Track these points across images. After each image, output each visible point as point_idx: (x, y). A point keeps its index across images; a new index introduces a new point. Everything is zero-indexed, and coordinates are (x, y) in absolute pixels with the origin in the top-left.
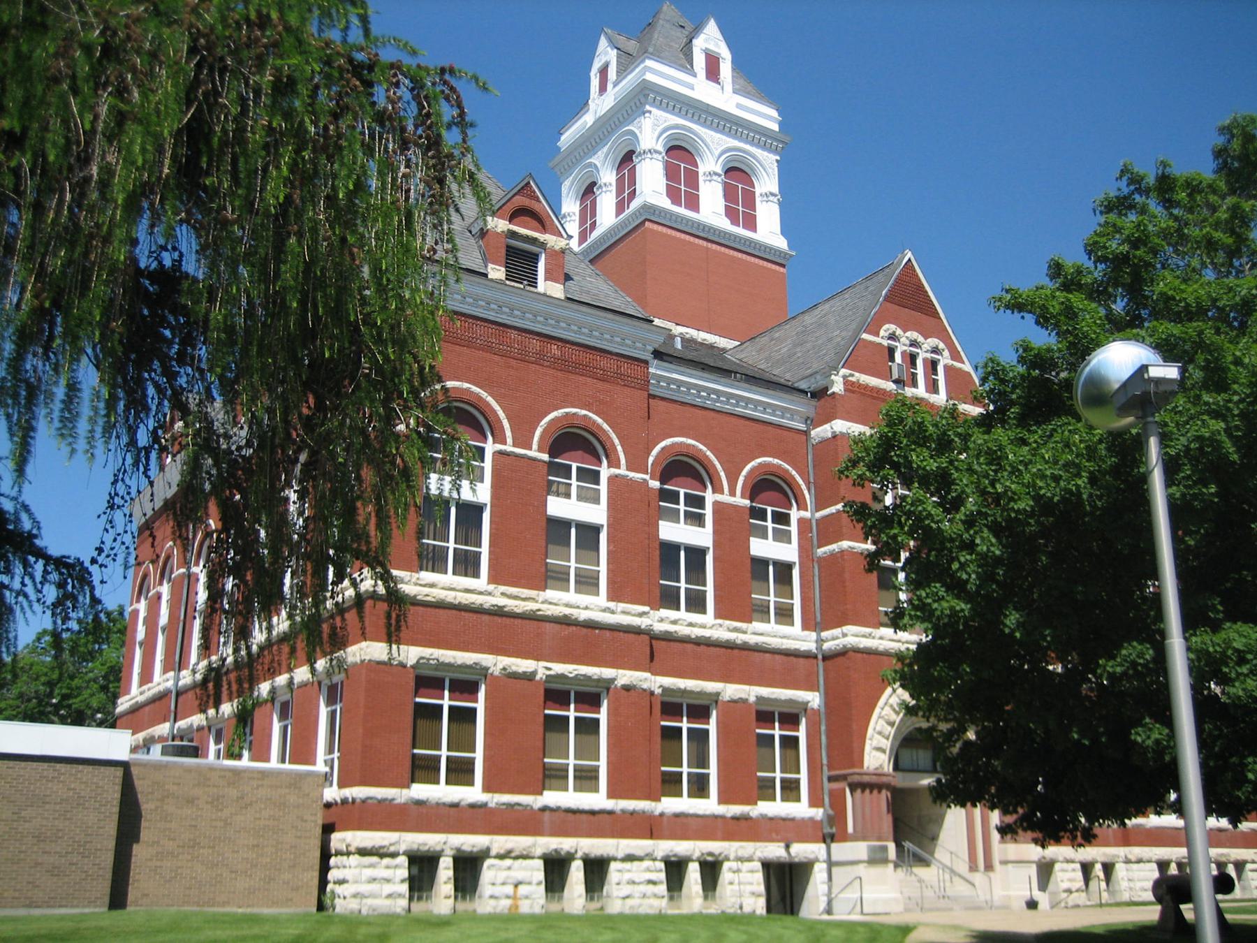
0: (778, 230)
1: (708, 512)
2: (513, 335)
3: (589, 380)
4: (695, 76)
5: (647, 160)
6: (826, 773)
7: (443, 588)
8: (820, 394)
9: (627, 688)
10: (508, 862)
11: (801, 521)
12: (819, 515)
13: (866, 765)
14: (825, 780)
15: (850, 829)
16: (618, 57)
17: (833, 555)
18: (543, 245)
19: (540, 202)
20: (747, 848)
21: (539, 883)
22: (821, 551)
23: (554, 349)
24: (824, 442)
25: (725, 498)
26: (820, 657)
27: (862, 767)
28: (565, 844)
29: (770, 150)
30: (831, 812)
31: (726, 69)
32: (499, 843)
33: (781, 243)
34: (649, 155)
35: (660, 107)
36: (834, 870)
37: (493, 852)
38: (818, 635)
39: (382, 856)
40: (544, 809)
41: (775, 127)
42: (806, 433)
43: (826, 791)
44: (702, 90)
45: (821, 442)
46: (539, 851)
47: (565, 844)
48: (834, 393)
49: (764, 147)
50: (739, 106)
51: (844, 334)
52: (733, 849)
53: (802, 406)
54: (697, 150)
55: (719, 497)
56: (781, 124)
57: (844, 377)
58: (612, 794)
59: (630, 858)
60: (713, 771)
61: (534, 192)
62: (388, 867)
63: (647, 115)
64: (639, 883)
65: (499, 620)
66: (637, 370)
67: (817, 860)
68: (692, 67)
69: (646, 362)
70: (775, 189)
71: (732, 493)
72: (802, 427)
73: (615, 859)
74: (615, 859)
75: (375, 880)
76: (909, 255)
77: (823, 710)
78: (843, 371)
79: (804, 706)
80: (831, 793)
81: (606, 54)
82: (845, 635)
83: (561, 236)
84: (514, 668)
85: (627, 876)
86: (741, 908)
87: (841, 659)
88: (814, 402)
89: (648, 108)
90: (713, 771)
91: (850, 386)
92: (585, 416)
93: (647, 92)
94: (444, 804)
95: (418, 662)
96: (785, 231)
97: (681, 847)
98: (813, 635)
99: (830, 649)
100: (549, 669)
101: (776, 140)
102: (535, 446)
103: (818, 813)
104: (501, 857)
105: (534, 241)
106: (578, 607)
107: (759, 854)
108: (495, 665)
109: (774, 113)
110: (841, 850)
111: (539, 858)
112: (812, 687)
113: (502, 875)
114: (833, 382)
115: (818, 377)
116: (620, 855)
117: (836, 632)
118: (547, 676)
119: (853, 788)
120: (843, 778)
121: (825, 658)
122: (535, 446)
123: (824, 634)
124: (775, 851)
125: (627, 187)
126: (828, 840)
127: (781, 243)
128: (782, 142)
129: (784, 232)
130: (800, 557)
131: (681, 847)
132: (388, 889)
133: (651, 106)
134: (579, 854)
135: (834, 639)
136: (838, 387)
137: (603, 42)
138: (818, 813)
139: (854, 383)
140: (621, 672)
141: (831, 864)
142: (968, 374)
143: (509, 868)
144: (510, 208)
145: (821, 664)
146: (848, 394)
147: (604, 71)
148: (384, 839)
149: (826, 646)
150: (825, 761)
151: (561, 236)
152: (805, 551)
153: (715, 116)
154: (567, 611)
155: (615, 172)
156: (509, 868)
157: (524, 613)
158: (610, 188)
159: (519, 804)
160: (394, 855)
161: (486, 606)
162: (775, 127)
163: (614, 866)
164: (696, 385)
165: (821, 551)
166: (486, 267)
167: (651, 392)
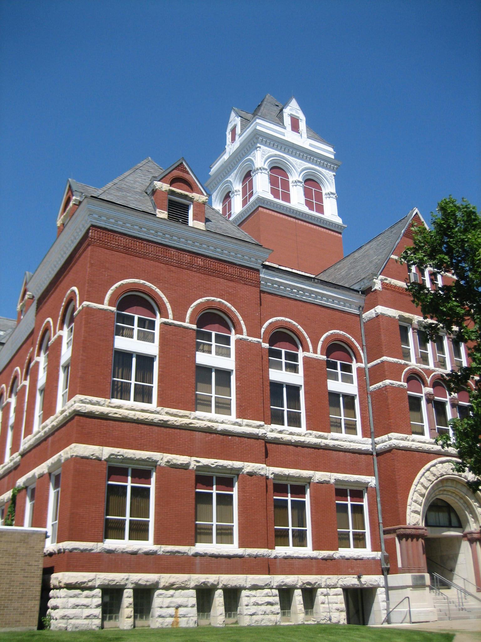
0: (337, 214)
1: (300, 363)
2: (173, 252)
3: (222, 280)
4: (285, 128)
5: (259, 174)
6: (382, 529)
7: (126, 409)
8: (367, 291)
9: (250, 474)
10: (171, 592)
11: (359, 369)
12: (369, 365)
13: (408, 522)
14: (382, 533)
15: (400, 565)
16: (241, 121)
17: (380, 389)
18: (191, 199)
19: (189, 174)
20: (333, 579)
21: (193, 606)
22: (372, 388)
23: (200, 261)
24: (371, 320)
25: (311, 355)
26: (374, 454)
27: (405, 524)
28: (211, 579)
29: (333, 170)
30: (386, 554)
31: (303, 125)
32: (166, 578)
33: (339, 221)
34: (260, 171)
35: (265, 145)
36: (390, 592)
37: (161, 585)
38: (373, 440)
39: (83, 589)
40: (196, 555)
41: (333, 157)
42: (359, 316)
43: (382, 541)
44: (290, 136)
45: (368, 321)
46: (192, 584)
47: (211, 579)
48: (376, 290)
49: (326, 168)
50: (311, 145)
51: (380, 257)
52: (324, 580)
53: (357, 299)
54: (288, 168)
55: (360, 365)
56: (335, 155)
57: (382, 280)
58: (241, 545)
59: (255, 587)
60: (309, 528)
61: (186, 168)
62: (87, 597)
63: (258, 149)
64: (261, 605)
65: (165, 430)
66: (252, 275)
67: (379, 586)
68: (283, 124)
69: (258, 270)
70: (334, 191)
71: (315, 352)
72: (357, 312)
73: (245, 588)
74: (245, 588)
75: (77, 606)
76: (416, 210)
77: (378, 488)
78: (381, 277)
79: (366, 486)
80: (386, 541)
81: (235, 120)
82: (390, 439)
83: (203, 194)
84: (175, 461)
85: (253, 600)
86: (330, 619)
87: (388, 455)
88: (363, 297)
89: (258, 145)
90: (309, 528)
91: (385, 286)
92: (219, 302)
93: (258, 136)
94: (127, 552)
95: (109, 457)
96: (341, 214)
97: (289, 579)
98: (370, 440)
99: (381, 448)
100: (198, 462)
101: (333, 163)
102: (187, 320)
103: (378, 555)
104: (167, 588)
105: (186, 197)
106: (217, 422)
107: (340, 583)
108: (162, 459)
109: (331, 150)
110: (394, 579)
111: (193, 589)
112: (370, 473)
113: (167, 601)
114: (375, 283)
115: (365, 281)
116: (248, 586)
117: (385, 437)
118: (197, 466)
119: (400, 537)
120: (394, 531)
121: (378, 455)
122: (187, 320)
123: (377, 439)
124: (351, 580)
125: (248, 190)
126: (385, 573)
127: (339, 221)
128: (336, 165)
129: (340, 215)
130: (359, 391)
131: (289, 579)
132: (87, 612)
133: (261, 144)
134: (220, 586)
135: (383, 442)
136: (378, 286)
137: (233, 114)
138: (378, 555)
139: (387, 284)
140: (246, 463)
141: (388, 588)
142: (222, 149)
143: (172, 596)
144: (170, 177)
145: (375, 458)
146: (385, 290)
147: (233, 130)
148: (84, 577)
149: (378, 447)
150: (381, 521)
151: (203, 194)
152: (362, 387)
153: (312, 155)
154: (210, 424)
155: (241, 184)
156: (172, 596)
157: (181, 425)
158: (238, 193)
159: (76, 549)
160: (91, 588)
161: (156, 421)
162: (333, 157)
163: (244, 593)
164: (290, 285)
165: (372, 388)
166: (155, 211)
167: (261, 289)
